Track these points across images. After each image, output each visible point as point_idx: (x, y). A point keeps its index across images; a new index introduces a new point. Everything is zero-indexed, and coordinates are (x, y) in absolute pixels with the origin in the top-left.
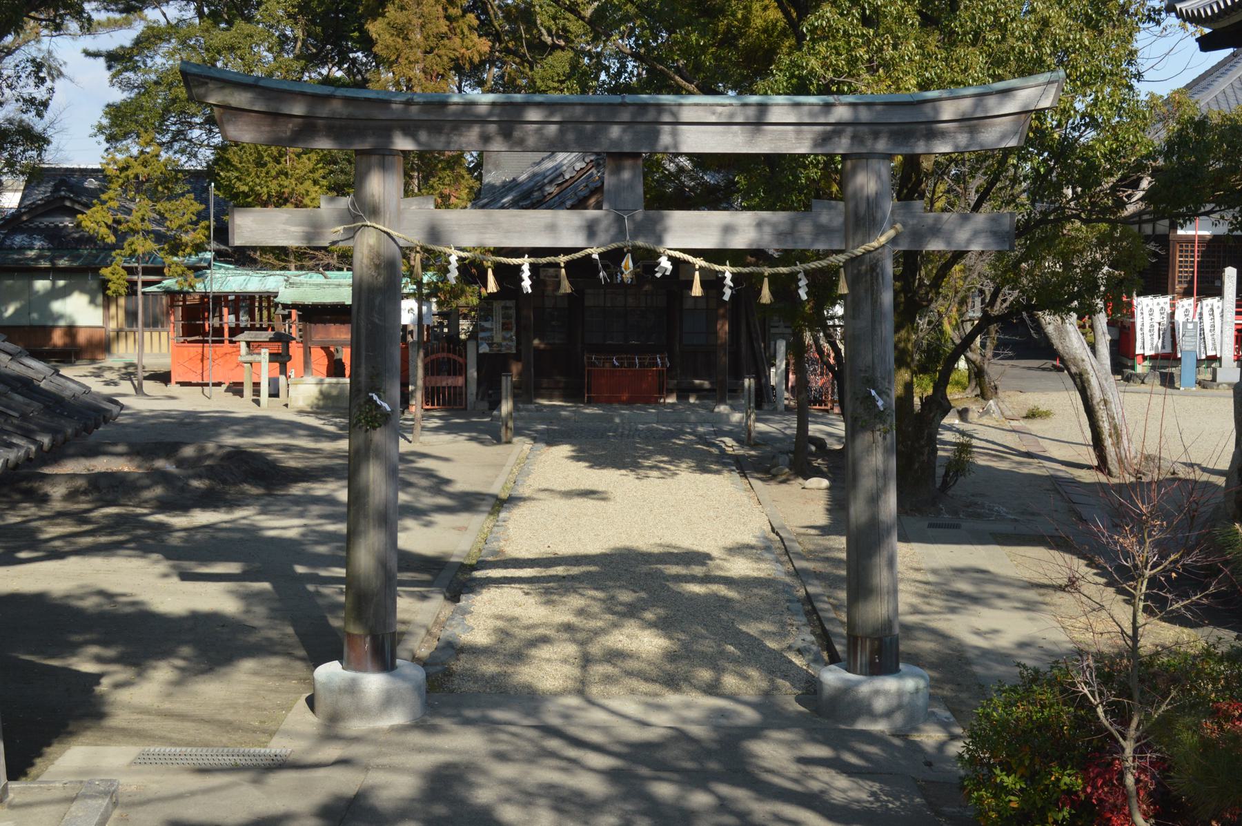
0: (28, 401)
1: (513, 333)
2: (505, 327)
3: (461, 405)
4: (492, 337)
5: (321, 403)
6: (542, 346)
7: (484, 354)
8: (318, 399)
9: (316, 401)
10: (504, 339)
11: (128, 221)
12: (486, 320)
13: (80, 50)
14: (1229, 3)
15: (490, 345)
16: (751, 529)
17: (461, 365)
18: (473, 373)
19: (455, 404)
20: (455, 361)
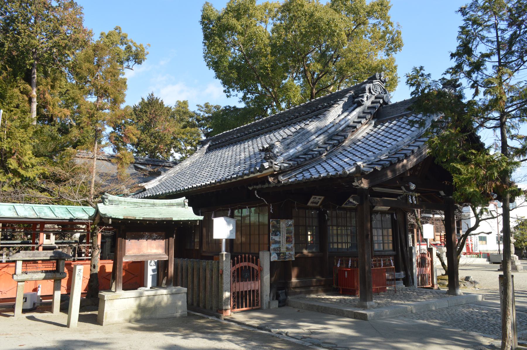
0: (100, 247)
1: (292, 245)
2: (288, 240)
3: (257, 305)
4: (280, 248)
5: (139, 317)
6: (310, 255)
7: (274, 262)
8: (136, 313)
9: (133, 315)
10: (288, 249)
11: (480, 99)
12: (276, 235)
13: (430, 73)
14: (1, 171)
15: (278, 255)
16: (488, 341)
17: (257, 271)
18: (267, 277)
19: (254, 306)
20: (253, 268)
